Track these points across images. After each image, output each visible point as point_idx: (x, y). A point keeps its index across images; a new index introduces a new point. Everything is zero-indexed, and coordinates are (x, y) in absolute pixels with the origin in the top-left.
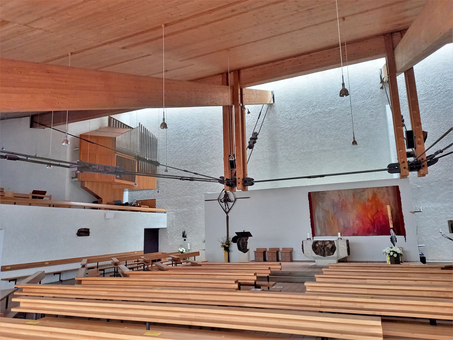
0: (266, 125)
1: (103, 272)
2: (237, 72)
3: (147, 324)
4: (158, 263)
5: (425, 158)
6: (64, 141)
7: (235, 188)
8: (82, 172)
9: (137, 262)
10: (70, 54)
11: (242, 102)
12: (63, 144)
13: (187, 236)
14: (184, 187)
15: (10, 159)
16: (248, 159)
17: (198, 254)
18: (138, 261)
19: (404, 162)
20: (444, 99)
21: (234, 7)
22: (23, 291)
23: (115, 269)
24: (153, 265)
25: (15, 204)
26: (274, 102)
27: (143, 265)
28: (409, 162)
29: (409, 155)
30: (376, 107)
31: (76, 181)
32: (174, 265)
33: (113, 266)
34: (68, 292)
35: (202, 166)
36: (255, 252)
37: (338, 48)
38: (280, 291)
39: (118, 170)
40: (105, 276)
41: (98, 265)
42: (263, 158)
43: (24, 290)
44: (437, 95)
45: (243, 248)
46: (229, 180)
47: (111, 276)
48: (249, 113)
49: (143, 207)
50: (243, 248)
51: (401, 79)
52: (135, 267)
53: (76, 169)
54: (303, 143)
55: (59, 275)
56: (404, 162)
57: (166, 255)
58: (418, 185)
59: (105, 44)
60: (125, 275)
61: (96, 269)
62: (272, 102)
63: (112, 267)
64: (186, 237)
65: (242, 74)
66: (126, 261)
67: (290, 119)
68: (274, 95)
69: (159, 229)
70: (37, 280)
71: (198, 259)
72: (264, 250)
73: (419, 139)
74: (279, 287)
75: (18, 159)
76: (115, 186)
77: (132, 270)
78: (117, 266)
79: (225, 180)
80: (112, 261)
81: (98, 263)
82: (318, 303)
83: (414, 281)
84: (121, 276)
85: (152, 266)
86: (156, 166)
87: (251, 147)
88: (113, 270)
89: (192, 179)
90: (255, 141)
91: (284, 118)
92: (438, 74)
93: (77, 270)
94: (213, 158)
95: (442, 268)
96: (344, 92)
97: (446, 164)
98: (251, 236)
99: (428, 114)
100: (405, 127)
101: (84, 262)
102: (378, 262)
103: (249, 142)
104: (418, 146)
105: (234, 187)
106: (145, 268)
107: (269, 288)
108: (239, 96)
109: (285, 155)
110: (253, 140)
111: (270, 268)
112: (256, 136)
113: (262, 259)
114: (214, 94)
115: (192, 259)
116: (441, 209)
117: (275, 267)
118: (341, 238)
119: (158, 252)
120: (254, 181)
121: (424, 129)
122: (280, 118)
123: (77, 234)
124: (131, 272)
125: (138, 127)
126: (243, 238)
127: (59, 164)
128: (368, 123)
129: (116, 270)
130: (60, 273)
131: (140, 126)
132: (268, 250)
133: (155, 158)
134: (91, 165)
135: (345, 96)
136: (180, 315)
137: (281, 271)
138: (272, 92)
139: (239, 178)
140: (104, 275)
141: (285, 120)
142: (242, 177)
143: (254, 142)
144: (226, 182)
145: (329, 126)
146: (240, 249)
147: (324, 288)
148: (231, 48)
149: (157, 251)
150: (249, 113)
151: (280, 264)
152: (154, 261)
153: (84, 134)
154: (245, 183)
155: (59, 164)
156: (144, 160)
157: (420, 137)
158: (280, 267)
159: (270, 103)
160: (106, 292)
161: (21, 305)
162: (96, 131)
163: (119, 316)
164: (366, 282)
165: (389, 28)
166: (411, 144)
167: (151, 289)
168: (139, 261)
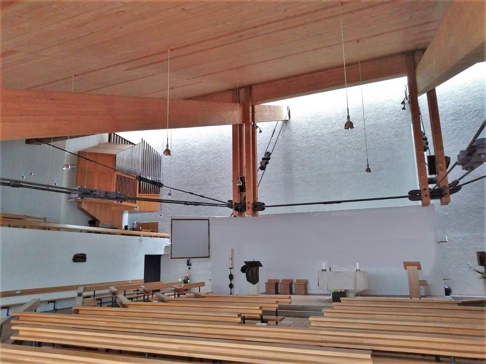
0: (281, 143)
1: (100, 302)
2: (249, 88)
3: (147, 355)
4: (159, 294)
5: (448, 186)
6: (65, 165)
7: (244, 213)
8: (82, 198)
9: (136, 292)
10: (73, 76)
11: (253, 120)
12: (64, 169)
13: (192, 264)
14: (190, 209)
15: (14, 186)
16: (259, 182)
17: (203, 284)
18: (138, 290)
19: (425, 189)
20: (474, 120)
21: (241, 34)
22: (20, 319)
23: (113, 298)
24: (154, 296)
25: (9, 226)
26: (290, 118)
27: (143, 295)
28: (430, 189)
29: (431, 181)
30: (401, 127)
31: (72, 202)
32: (176, 296)
33: (111, 296)
34: (65, 321)
35: (210, 187)
36: (267, 284)
37: (358, 65)
38: (289, 326)
39: (119, 196)
40: (102, 306)
41: (94, 293)
42: (277, 180)
43: (21, 318)
44: (466, 114)
45: (253, 279)
46: (238, 204)
47: (108, 306)
48: (261, 131)
49: (144, 231)
50: (253, 279)
51: (423, 100)
52: (135, 297)
53: (77, 195)
54: (321, 164)
55: (53, 303)
56: (425, 189)
57: (169, 285)
58: (446, 212)
59: (109, 67)
60: (124, 306)
61: (92, 298)
62: (287, 118)
63: (109, 296)
64: (191, 265)
65: (255, 90)
66: (125, 291)
67: (308, 137)
68: (289, 110)
69: (161, 255)
70: (33, 308)
71: (204, 290)
72: (276, 282)
73: (441, 165)
74: (289, 322)
75: (22, 186)
76: (114, 208)
77: (131, 300)
78: (115, 296)
79: (233, 204)
80: (110, 290)
81: (94, 292)
82: (319, 338)
83: (424, 317)
84: (119, 307)
85: (152, 296)
86: (160, 188)
87: (263, 168)
88: (111, 300)
89: (197, 204)
90: (267, 161)
91: (300, 136)
92: (468, 92)
93: (74, 298)
94: (223, 178)
95: (459, 304)
96: (349, 125)
97: (476, 189)
98: (261, 266)
99: (456, 135)
100: (429, 150)
101: (81, 290)
102: (400, 296)
103: (261, 163)
104: (441, 173)
105: (243, 212)
106: (145, 298)
107: (277, 323)
108: (251, 114)
109: (301, 176)
110: (265, 161)
111: (277, 302)
112: (269, 156)
113: (273, 291)
114: (223, 113)
115: (196, 290)
116: (469, 239)
117: (284, 299)
118: (359, 270)
119: (160, 281)
120: (265, 205)
121: (446, 154)
122: (296, 136)
123: (73, 260)
124: (129, 302)
125: (141, 143)
126: (252, 268)
127: (58, 190)
128: (392, 144)
129: (114, 300)
130: (55, 301)
131: (142, 142)
132: (281, 281)
133: (158, 178)
134: (92, 191)
135: (350, 129)
136: (179, 347)
137: (290, 304)
138: (288, 108)
139: (249, 203)
140: (101, 304)
141: (301, 138)
142: (252, 202)
143: (267, 163)
144: (235, 206)
145: (350, 146)
146: (249, 280)
147: (329, 323)
148: (240, 67)
149: (159, 280)
150: (261, 131)
151: (290, 298)
152: (154, 291)
153: (83, 150)
154: (255, 207)
155: (58, 190)
156: (146, 180)
157: (442, 163)
158: (289, 300)
159: (286, 119)
160: (105, 323)
161: (21, 333)
162: (96, 147)
163: (118, 347)
164: (375, 317)
165: (410, 47)
166: (432, 171)
167: (150, 320)
168: (139, 291)
